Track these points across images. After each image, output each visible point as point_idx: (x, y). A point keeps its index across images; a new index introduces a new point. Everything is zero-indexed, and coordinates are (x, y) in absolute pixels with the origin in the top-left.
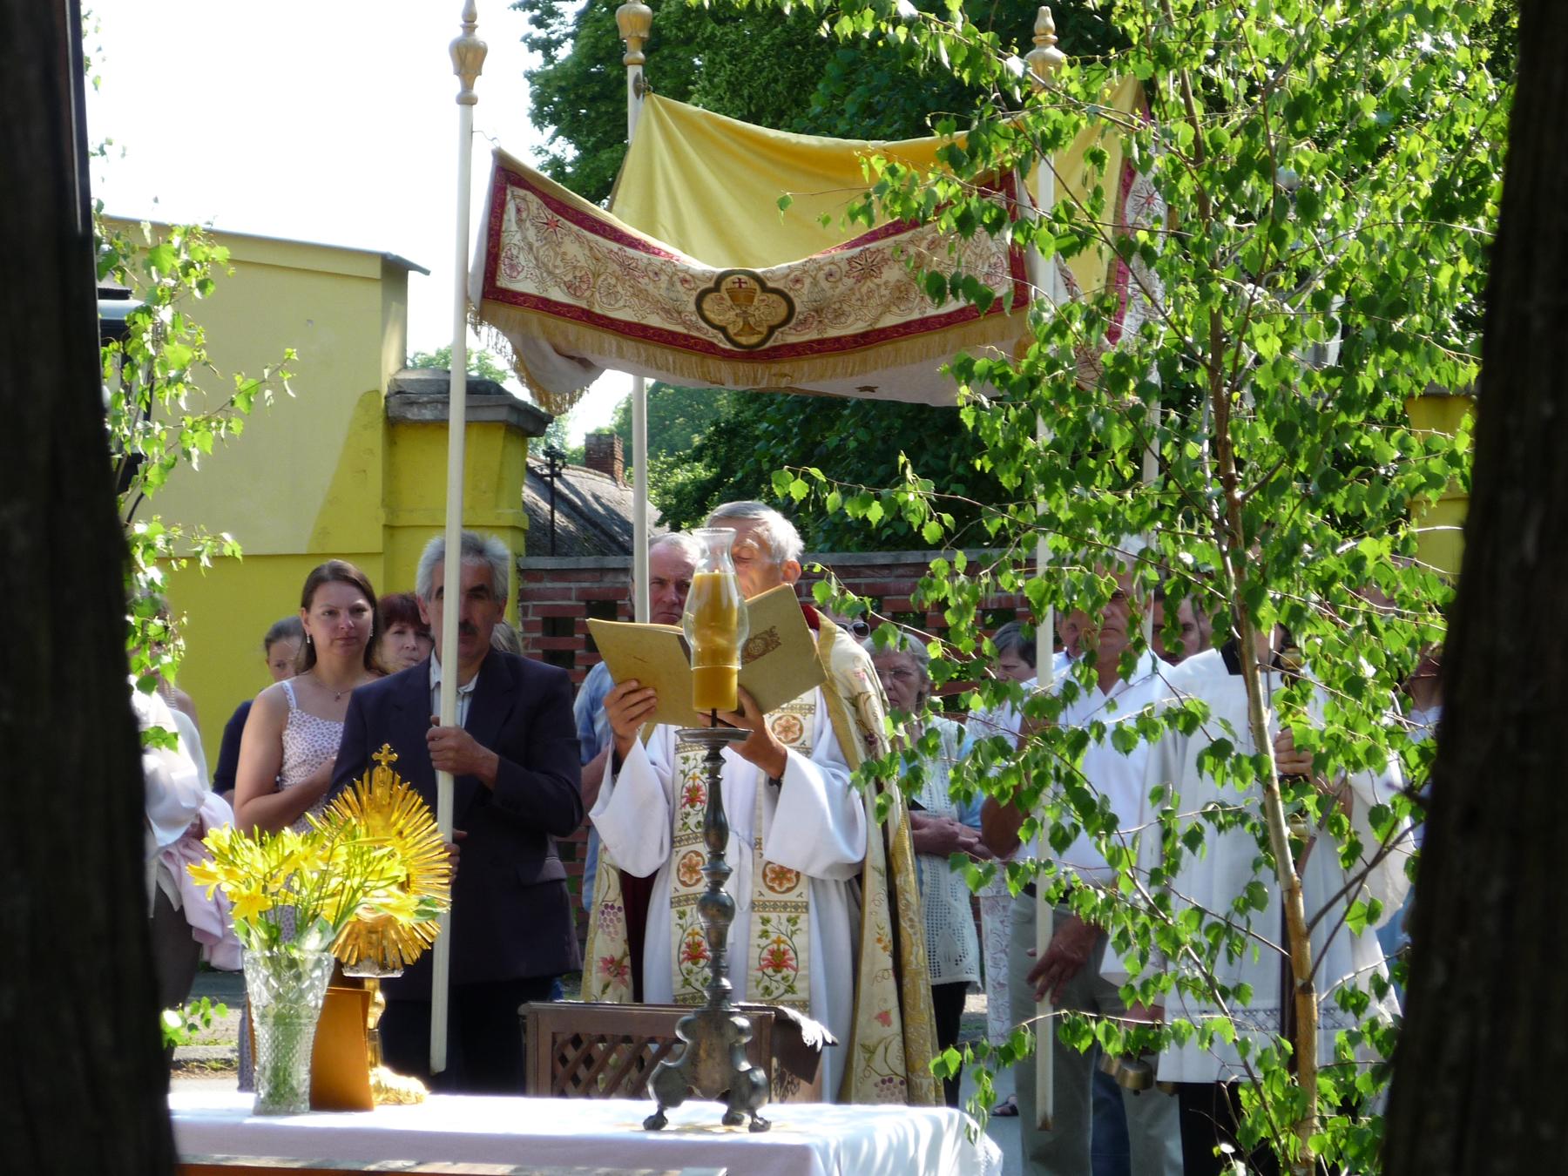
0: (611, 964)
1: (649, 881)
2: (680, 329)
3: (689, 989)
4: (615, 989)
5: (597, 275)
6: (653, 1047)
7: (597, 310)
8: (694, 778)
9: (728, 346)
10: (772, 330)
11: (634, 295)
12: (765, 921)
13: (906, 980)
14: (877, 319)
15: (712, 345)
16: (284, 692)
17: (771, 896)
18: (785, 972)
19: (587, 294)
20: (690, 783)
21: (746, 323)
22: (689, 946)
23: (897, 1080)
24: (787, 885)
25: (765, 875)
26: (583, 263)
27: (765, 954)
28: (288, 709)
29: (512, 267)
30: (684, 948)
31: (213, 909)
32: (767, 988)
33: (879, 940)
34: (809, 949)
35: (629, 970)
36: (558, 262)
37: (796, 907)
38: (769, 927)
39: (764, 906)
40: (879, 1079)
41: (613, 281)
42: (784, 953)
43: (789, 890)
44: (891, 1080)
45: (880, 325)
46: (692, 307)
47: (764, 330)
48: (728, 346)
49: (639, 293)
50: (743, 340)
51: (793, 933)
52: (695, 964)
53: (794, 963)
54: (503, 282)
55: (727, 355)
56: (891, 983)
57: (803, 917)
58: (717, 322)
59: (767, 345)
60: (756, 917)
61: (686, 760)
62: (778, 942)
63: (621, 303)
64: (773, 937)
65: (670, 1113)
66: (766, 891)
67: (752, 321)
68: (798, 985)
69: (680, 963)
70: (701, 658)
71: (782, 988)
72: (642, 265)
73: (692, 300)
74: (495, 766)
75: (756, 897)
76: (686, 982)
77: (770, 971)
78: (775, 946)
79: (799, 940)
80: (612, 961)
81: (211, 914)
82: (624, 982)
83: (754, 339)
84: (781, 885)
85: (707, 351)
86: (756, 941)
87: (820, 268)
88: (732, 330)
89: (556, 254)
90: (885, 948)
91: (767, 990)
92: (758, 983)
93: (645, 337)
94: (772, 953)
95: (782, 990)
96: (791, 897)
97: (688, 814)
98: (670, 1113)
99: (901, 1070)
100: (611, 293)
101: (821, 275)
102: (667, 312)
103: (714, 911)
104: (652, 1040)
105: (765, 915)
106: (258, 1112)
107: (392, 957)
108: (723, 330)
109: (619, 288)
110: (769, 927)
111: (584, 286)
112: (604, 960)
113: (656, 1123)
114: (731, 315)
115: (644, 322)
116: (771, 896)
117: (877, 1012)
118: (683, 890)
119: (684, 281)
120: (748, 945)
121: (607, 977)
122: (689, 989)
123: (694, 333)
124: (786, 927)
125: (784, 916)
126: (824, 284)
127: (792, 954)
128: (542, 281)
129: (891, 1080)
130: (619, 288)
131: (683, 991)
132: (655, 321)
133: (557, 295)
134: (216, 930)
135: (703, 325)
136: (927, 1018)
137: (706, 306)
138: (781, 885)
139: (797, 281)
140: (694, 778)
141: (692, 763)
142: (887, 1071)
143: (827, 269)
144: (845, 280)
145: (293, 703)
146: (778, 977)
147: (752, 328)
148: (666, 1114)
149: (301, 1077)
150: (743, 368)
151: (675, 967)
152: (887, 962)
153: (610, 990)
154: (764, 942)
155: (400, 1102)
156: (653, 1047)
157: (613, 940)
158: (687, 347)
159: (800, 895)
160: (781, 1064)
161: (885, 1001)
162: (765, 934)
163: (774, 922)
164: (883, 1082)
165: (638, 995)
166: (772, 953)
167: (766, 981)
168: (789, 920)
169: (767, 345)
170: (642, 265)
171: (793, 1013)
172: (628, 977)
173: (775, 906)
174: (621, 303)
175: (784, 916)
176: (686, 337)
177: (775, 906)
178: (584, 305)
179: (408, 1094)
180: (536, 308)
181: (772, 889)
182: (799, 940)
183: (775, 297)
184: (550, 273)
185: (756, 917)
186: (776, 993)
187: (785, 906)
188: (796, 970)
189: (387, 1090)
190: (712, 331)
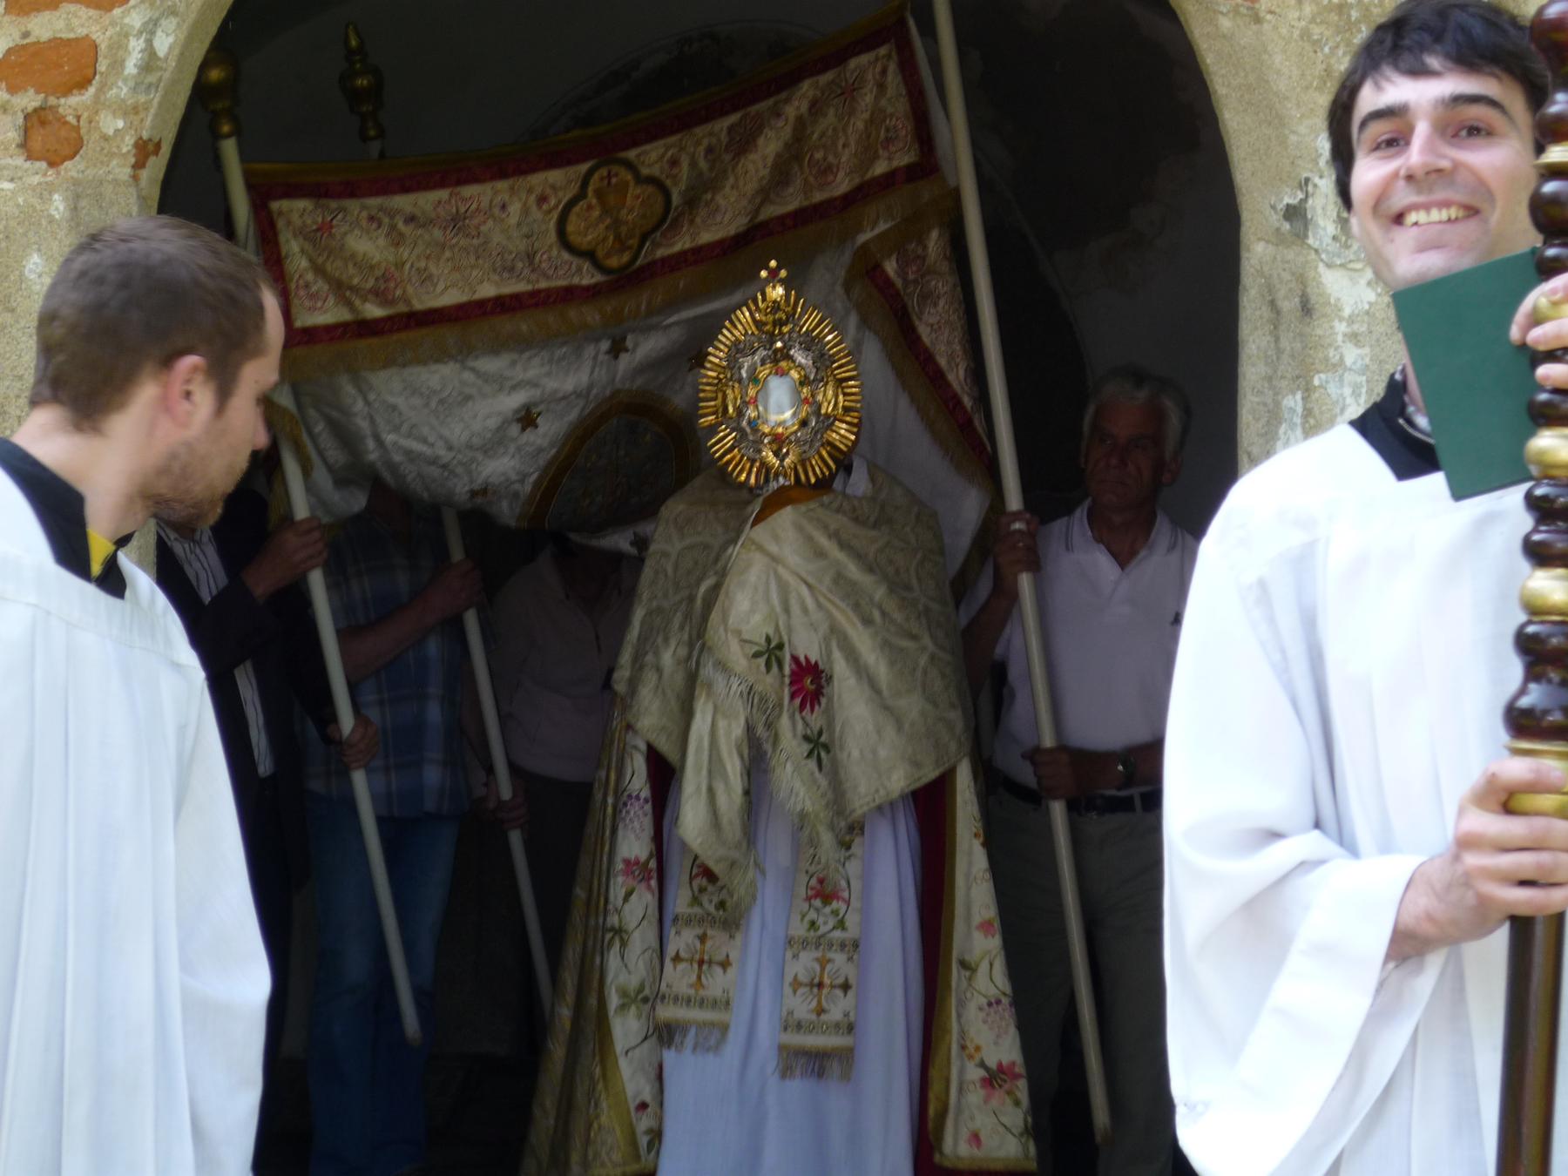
7: (418, 306)
14: (757, 211)
18: (835, 905)
21: (618, 238)
32: (813, 923)
40: (984, 1001)
41: (422, 264)
44: (998, 1002)
45: (762, 217)
53: (846, 895)
59: (638, 263)
71: (832, 923)
77: (817, 903)
83: (626, 258)
91: (813, 923)
92: (803, 916)
95: (831, 925)
115: (477, 296)
136: (1253, 292)
146: (828, 910)
153: (634, 897)
158: (536, 305)
164: (990, 1004)
167: (812, 915)
169: (638, 263)
172: (653, 883)
176: (534, 294)
178: (402, 308)
183: (650, 189)
186: (823, 929)
188: (848, 904)
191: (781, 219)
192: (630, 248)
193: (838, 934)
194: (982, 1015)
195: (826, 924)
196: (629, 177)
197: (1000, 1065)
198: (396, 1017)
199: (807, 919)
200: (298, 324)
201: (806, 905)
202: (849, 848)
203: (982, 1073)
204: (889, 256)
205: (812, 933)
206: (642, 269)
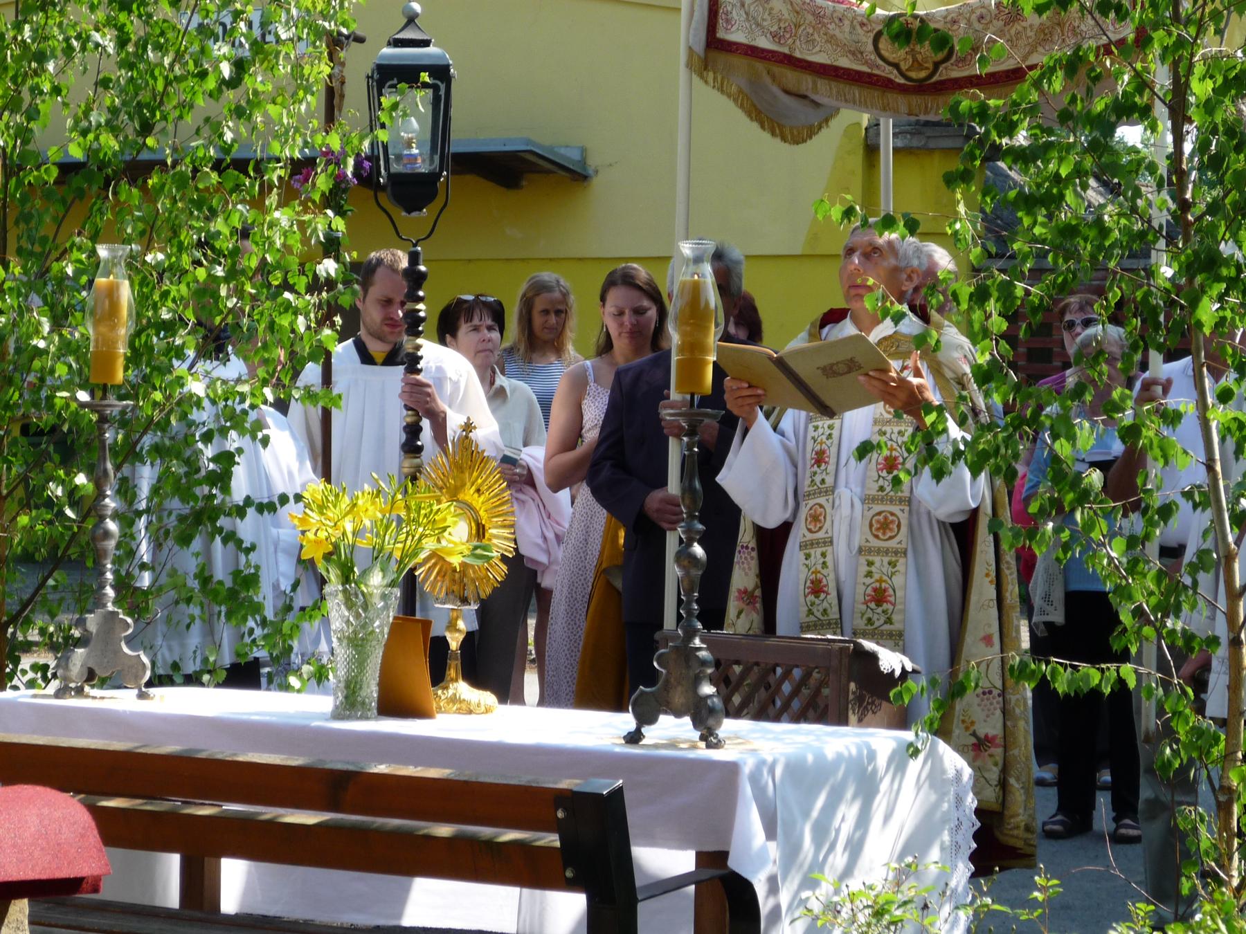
0: (746, 595)
1: (786, 527)
2: (865, 69)
3: (812, 618)
4: (747, 615)
5: (797, 26)
6: (737, 669)
7: (798, 55)
8: (821, 443)
9: (902, 81)
10: (937, 65)
11: (827, 41)
12: (870, 564)
13: (1004, 612)
15: (890, 81)
16: (585, 370)
17: (875, 543)
18: (885, 606)
19: (790, 41)
20: (818, 448)
21: (915, 60)
22: (812, 582)
23: (996, 692)
24: (889, 534)
25: (871, 525)
26: (786, 16)
27: (869, 591)
28: (586, 383)
29: (728, 21)
30: (808, 584)
31: (540, 541)
32: (869, 620)
33: (987, 575)
34: (905, 588)
35: (759, 600)
36: (766, 16)
37: (896, 553)
38: (873, 569)
39: (870, 551)
41: (811, 31)
42: (885, 590)
43: (891, 538)
44: (990, 692)
46: (870, 47)
47: (930, 65)
48: (902, 81)
49: (831, 39)
50: (913, 75)
51: (893, 574)
52: (817, 597)
53: (892, 599)
54: (721, 34)
55: (902, 89)
56: (994, 612)
57: (902, 560)
58: (891, 60)
59: (935, 79)
60: (863, 560)
61: (816, 428)
62: (880, 581)
63: (818, 48)
64: (876, 576)
65: (646, 730)
66: (871, 538)
67: (919, 57)
68: (895, 617)
69: (806, 596)
70: (72, 413)
72: (828, 13)
73: (870, 41)
74: (715, 433)
75: (863, 543)
76: (810, 612)
77: (873, 605)
78: (877, 585)
79: (898, 581)
80: (745, 592)
81: (538, 545)
82: (754, 608)
83: (923, 74)
84: (884, 534)
85: (886, 86)
86: (862, 579)
87: (973, 12)
88: (904, 66)
89: (764, 9)
90: (991, 582)
91: (869, 620)
92: (863, 615)
93: (837, 76)
94: (875, 590)
95: (882, 621)
96: (892, 544)
97: (815, 473)
98: (646, 730)
99: (999, 684)
100: (810, 41)
101: (974, 17)
102: (854, 54)
103: (686, 563)
104: (738, 662)
105: (871, 558)
106: (337, 715)
107: (469, 592)
108: (896, 66)
109: (816, 36)
110: (873, 569)
111: (788, 36)
112: (739, 591)
113: (634, 738)
114: (902, 53)
115: (836, 64)
116: (875, 543)
117: (982, 634)
118: (809, 536)
119: (862, 24)
120: (855, 584)
121: (742, 605)
122: (812, 618)
123: (876, 72)
124: (886, 569)
125: (886, 560)
126: (977, 26)
127: (891, 591)
128: (751, 31)
129: (990, 692)
130: (816, 36)
131: (807, 620)
132: (845, 62)
133: (764, 43)
134: (543, 558)
135: (881, 63)
137: (882, 45)
138: (884, 534)
139: (954, 22)
140: (821, 443)
141: (820, 431)
142: (988, 685)
143: (978, 12)
144: (995, 22)
145: (591, 378)
146: (880, 610)
147: (920, 65)
148: (643, 730)
149: (371, 690)
150: (916, 100)
151: (802, 599)
152: (993, 593)
153: (743, 615)
154: (868, 581)
155: (470, 712)
156: (737, 669)
157: (746, 574)
159: (900, 543)
160: (860, 686)
161: (990, 626)
162: (869, 574)
163: (877, 564)
165: (769, 624)
166: (875, 590)
167: (869, 614)
168: (889, 564)
169: (935, 79)
170: (828, 13)
171: (869, 645)
173: (879, 551)
174: (818, 48)
175: (886, 560)
176: (870, 75)
177: (879, 551)
178: (786, 50)
179: (479, 705)
180: (746, 54)
181: (877, 537)
182: (898, 581)
184: (758, 25)
185: (863, 560)
186: (877, 624)
187: (887, 552)
188: (894, 605)
189: (461, 701)
190: (888, 68)
192: (927, 68)
193: (887, 627)
195: (879, 621)
197: (986, 736)
199: (866, 616)
200: (392, 170)
201: (864, 607)
202: (895, 566)
203: (973, 740)
204: (139, 588)
205: (869, 627)
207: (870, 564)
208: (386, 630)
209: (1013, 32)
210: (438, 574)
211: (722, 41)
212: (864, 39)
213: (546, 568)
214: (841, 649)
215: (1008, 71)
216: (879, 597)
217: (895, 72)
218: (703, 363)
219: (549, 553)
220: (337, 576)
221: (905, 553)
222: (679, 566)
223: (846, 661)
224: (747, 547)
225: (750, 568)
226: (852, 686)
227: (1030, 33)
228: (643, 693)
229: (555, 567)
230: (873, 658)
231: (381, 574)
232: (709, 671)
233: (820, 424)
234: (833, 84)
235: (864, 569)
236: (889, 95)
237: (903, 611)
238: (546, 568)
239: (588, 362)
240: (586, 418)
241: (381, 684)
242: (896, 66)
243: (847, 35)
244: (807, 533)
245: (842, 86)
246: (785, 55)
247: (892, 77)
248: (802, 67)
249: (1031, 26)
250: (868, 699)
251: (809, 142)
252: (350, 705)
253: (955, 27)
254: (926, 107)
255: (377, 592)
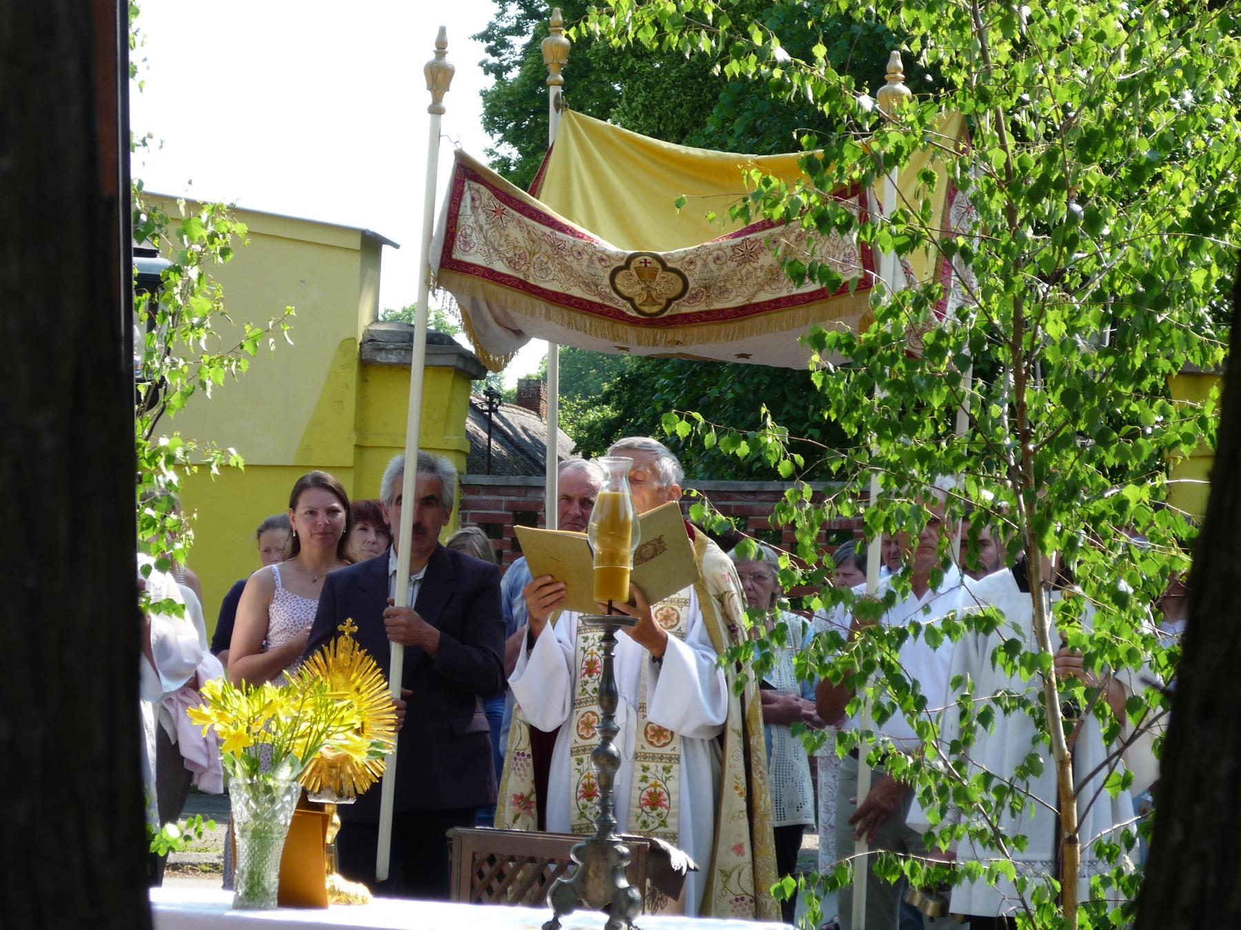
0: (521, 800)
2: (596, 299)
3: (584, 821)
4: (524, 820)
5: (532, 254)
7: (531, 281)
8: (592, 654)
9: (634, 314)
11: (561, 270)
12: (645, 769)
13: (756, 820)
15: (622, 313)
19: (525, 268)
20: (589, 658)
21: (650, 296)
22: (585, 786)
24: (663, 741)
25: (646, 733)
27: (644, 795)
28: (274, 587)
30: (581, 787)
31: (202, 744)
32: (645, 822)
35: (534, 805)
36: (502, 242)
37: (670, 759)
38: (648, 774)
39: (645, 757)
40: (733, 897)
41: (545, 259)
42: (660, 794)
43: (665, 745)
44: (742, 899)
46: (607, 281)
47: (664, 302)
48: (634, 314)
49: (565, 269)
50: (646, 309)
51: (667, 779)
52: (590, 800)
53: (667, 803)
54: (457, 255)
55: (633, 321)
57: (675, 767)
59: (666, 314)
60: (638, 765)
61: (586, 639)
62: (655, 785)
63: (551, 277)
64: (651, 781)
66: (646, 745)
67: (654, 294)
68: (669, 820)
69: (577, 800)
72: (568, 246)
73: (607, 276)
74: (437, 639)
75: (639, 750)
76: (582, 815)
77: (648, 809)
79: (672, 785)
80: (522, 797)
81: (199, 748)
82: (530, 814)
83: (655, 309)
84: (658, 740)
85: (617, 318)
86: (637, 784)
88: (637, 301)
91: (645, 822)
92: (638, 818)
93: (569, 304)
94: (650, 794)
95: (657, 824)
96: (666, 750)
97: (586, 682)
100: (543, 269)
102: (587, 285)
104: (552, 861)
105: (645, 764)
106: (239, 905)
107: (347, 787)
108: (630, 300)
109: (550, 265)
110: (648, 774)
111: (522, 262)
112: (515, 796)
118: (582, 742)
119: (601, 260)
121: (517, 809)
122: (584, 821)
125: (660, 765)
126: (712, 266)
127: (665, 796)
128: (489, 256)
131: (579, 822)
132: (577, 292)
133: (500, 267)
134: (203, 762)
135: (615, 295)
138: (658, 740)
140: (592, 654)
141: (591, 642)
143: (715, 254)
144: (729, 263)
145: (279, 583)
146: (654, 814)
148: (560, 920)
149: (272, 880)
151: (573, 803)
154: (643, 785)
155: (349, 903)
157: (523, 780)
159: (674, 749)
160: (653, 884)
162: (644, 779)
163: (652, 770)
164: (737, 900)
165: (542, 824)
166: (650, 794)
167: (644, 817)
169: (666, 314)
170: (568, 246)
171: (664, 844)
172: (534, 810)
173: (654, 757)
174: (551, 277)
175: (660, 765)
176: (601, 306)
177: (654, 757)
179: (356, 897)
180: (483, 276)
181: (651, 743)
182: (672, 785)
184: (495, 250)
185: (638, 765)
186: (652, 827)
187: (661, 758)
188: (668, 808)
189: (340, 893)
191: (722, 311)
193: (661, 829)
194: (731, 906)
196: (659, 266)
198: (652, 515)
206: (672, 317)
207: (645, 769)
208: (289, 822)
209: (744, 272)
210: (313, 769)
211: (458, 262)
212: (602, 274)
213: (204, 770)
214: (639, 846)
215: (736, 308)
216: (654, 801)
217: (629, 305)
218: (622, 572)
219: (208, 756)
220: (244, 770)
221: (678, 759)
222: (597, 763)
223: (643, 858)
224: (523, 754)
225: (526, 775)
226: (648, 882)
227: (759, 274)
228: (561, 884)
229: (214, 771)
230: (665, 855)
231: (289, 769)
232: (626, 864)
233: (590, 635)
234: (565, 312)
235: (640, 774)
236: (620, 326)
237: (678, 815)
238: (204, 770)
239: (275, 567)
240: (273, 622)
241: (282, 877)
242: (630, 300)
243: (584, 268)
244: (578, 739)
245: (573, 314)
246: (521, 281)
247: (624, 310)
248: (535, 293)
249: (762, 267)
250: (658, 896)
251: (509, 365)
252: (253, 897)
253: (692, 267)
254: (655, 340)
255: (284, 786)
